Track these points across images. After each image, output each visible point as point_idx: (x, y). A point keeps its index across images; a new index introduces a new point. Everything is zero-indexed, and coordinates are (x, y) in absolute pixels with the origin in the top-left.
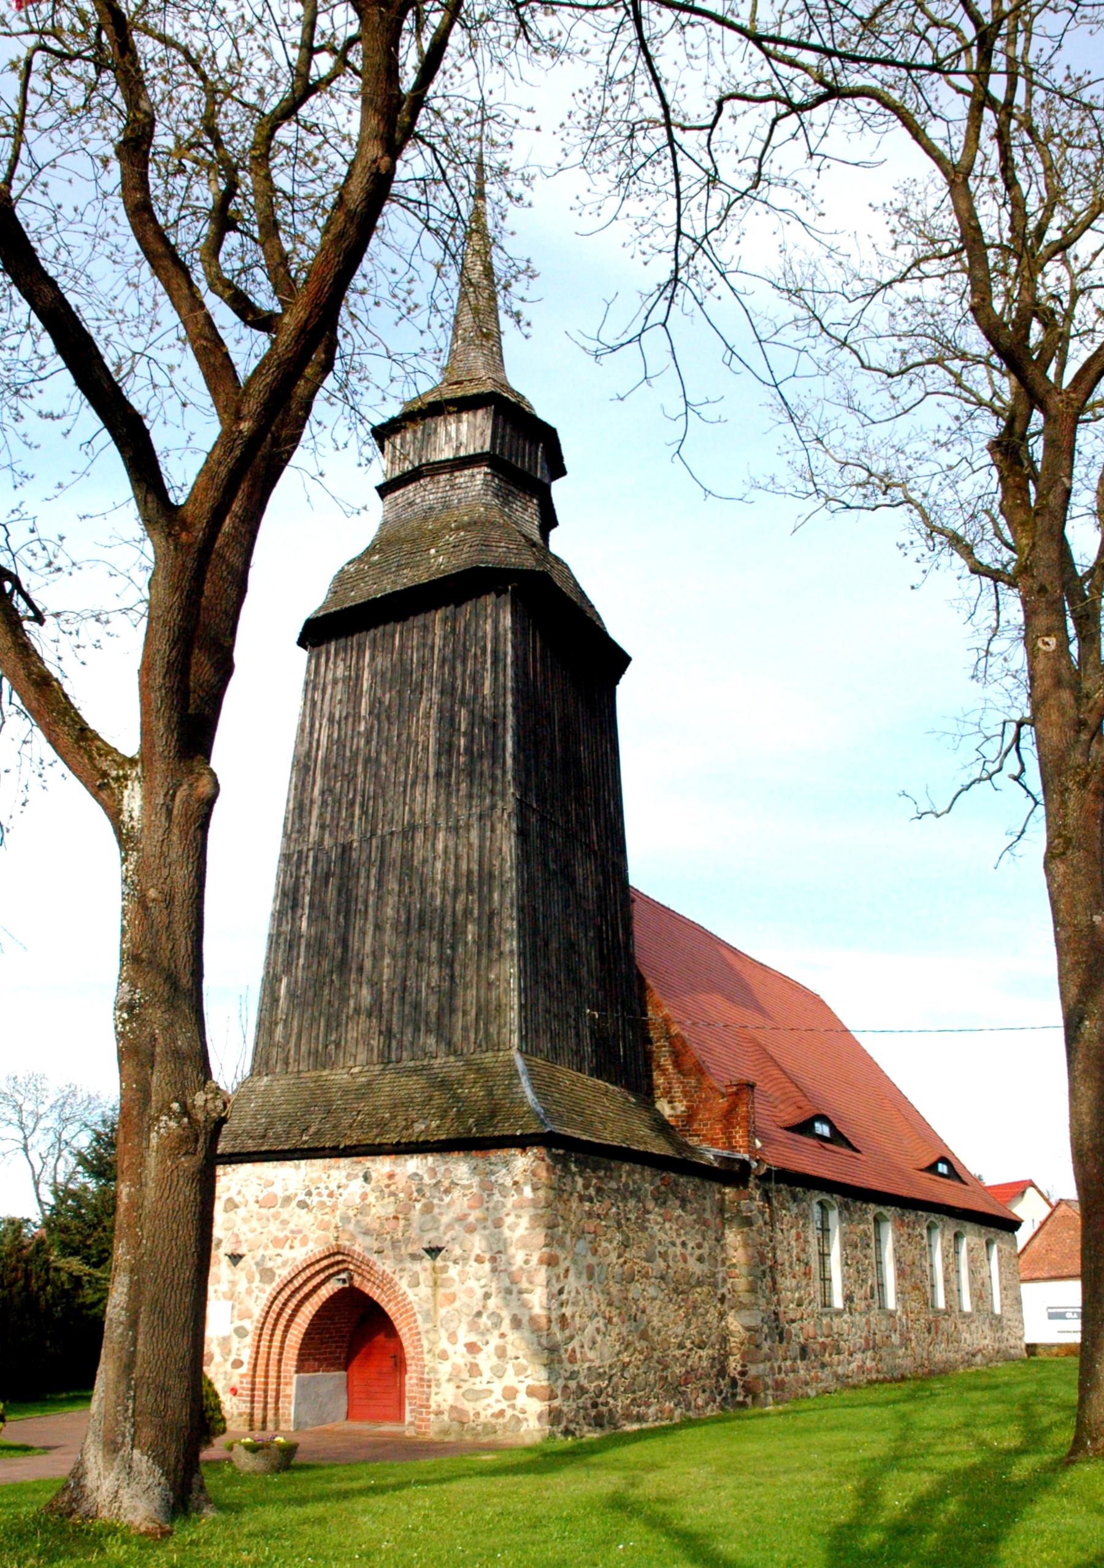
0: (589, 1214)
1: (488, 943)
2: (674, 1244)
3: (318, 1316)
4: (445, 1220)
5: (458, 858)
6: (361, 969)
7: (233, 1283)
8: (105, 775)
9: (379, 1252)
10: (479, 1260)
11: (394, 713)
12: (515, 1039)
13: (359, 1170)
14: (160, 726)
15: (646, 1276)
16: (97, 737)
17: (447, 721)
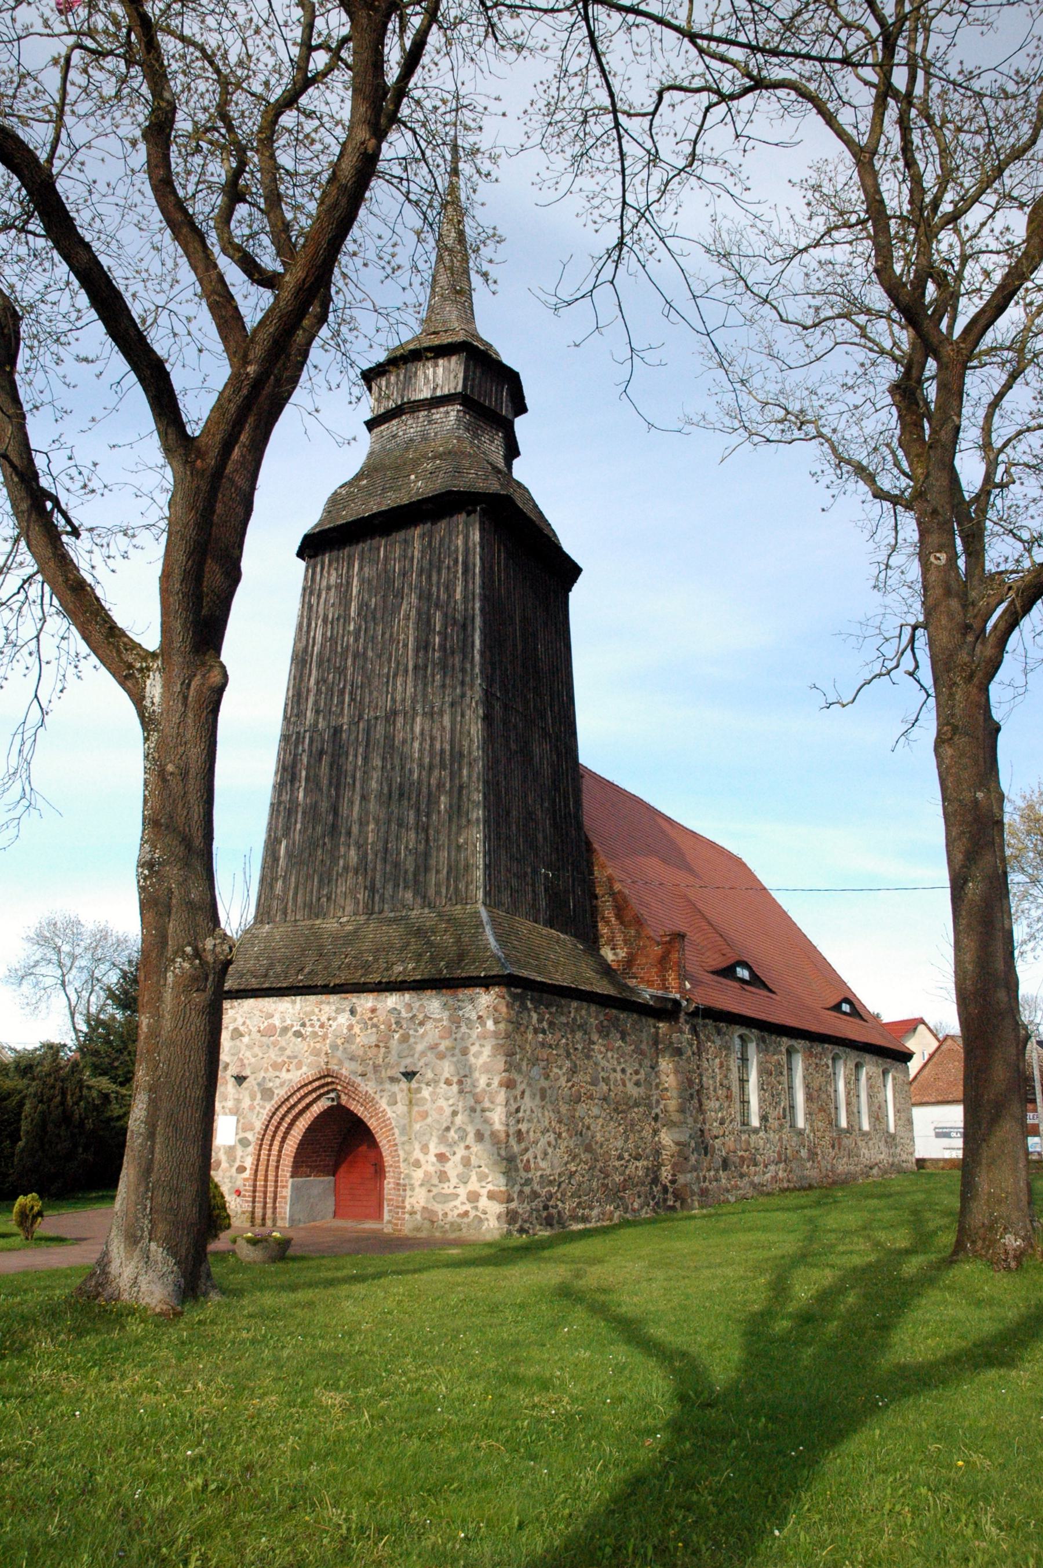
0: (543, 1045)
1: (457, 811)
2: (615, 1071)
3: (310, 1130)
4: (420, 1048)
5: (432, 739)
6: (349, 833)
7: (238, 1101)
8: (130, 666)
9: (363, 1075)
10: (448, 1083)
11: (379, 615)
12: (480, 894)
13: (346, 1006)
14: (178, 625)
15: (591, 1097)
16: (123, 634)
17: (425, 623)
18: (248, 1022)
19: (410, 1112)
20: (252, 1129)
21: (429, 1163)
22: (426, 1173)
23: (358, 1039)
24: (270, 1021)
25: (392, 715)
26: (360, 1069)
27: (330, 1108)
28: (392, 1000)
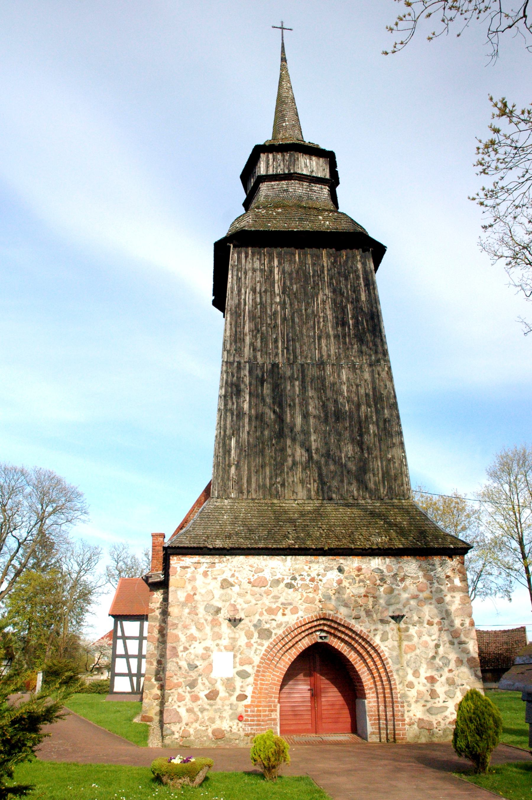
9: (357, 618)
10: (430, 623)
18: (236, 574)
19: (400, 646)
20: (250, 663)
21: (421, 685)
22: (419, 692)
23: (348, 591)
24: (260, 575)
25: (321, 365)
26: (354, 613)
27: (317, 643)
28: (376, 562)
